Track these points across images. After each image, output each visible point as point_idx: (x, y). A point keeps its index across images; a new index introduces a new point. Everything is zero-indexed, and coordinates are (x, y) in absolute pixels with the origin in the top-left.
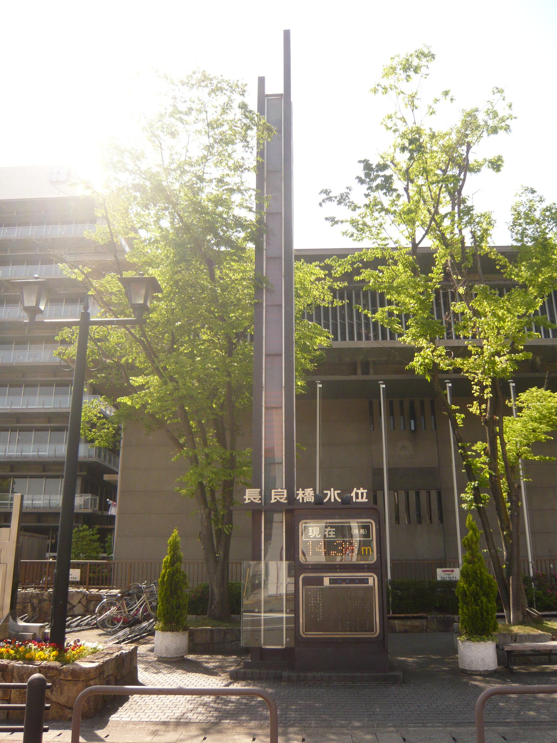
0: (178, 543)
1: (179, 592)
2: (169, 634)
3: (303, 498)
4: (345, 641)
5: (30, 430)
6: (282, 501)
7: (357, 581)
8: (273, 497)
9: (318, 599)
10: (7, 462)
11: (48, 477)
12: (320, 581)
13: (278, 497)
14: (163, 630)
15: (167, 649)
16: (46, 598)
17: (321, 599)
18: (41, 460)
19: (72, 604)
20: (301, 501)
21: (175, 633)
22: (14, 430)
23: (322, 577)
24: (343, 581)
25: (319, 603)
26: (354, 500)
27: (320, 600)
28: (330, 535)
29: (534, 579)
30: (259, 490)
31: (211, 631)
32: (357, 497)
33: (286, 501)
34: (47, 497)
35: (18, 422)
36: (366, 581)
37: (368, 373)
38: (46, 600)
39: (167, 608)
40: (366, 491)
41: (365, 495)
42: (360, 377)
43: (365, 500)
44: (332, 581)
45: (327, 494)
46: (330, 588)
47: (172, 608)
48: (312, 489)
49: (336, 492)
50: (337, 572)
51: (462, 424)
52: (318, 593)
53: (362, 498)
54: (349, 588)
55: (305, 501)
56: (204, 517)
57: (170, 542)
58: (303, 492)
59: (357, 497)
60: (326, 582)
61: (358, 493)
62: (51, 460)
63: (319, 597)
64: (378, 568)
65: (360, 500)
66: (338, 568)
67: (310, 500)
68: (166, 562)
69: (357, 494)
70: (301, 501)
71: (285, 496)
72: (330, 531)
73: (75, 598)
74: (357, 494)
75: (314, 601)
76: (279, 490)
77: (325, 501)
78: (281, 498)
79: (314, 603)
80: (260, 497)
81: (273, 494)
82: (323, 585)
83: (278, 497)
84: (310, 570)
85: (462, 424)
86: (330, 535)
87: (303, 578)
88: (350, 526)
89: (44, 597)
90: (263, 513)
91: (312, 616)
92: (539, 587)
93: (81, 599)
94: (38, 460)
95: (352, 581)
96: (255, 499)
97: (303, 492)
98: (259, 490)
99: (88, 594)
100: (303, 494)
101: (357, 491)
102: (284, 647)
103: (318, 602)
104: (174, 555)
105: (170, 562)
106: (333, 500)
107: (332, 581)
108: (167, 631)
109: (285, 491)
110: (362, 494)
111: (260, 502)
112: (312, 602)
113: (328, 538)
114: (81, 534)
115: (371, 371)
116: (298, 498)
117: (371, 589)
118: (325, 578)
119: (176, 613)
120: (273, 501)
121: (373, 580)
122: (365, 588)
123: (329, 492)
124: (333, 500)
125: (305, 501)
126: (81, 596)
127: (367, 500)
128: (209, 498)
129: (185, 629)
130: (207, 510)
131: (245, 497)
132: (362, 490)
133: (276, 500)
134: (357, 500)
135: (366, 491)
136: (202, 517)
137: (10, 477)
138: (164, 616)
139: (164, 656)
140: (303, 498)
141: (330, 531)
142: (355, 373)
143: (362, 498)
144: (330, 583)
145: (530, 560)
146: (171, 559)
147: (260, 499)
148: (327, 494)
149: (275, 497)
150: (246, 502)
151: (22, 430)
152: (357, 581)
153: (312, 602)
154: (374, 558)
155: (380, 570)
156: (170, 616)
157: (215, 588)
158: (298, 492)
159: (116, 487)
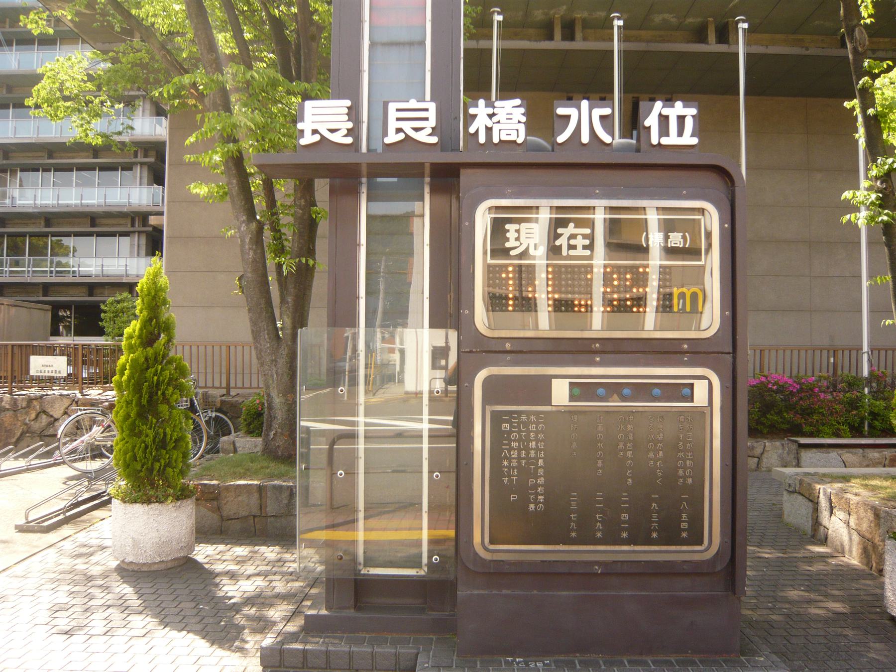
0: (162, 289)
1: (163, 408)
2: (138, 508)
3: (489, 130)
4: (614, 571)
5: (68, 168)
6: (423, 137)
7: (657, 392)
8: (393, 125)
9: (533, 444)
10: (39, 213)
11: (100, 234)
12: (540, 390)
13: (407, 126)
14: (129, 499)
15: (136, 544)
16: (8, 407)
17: (541, 445)
18: (87, 209)
19: (52, 416)
20: (482, 139)
21: (154, 506)
22: (46, 169)
23: (548, 379)
24: (614, 389)
25: (537, 459)
26: (654, 140)
27: (537, 449)
28: (574, 247)
29: (869, 381)
30: (348, 103)
31: (260, 489)
32: (664, 130)
33: (434, 140)
34: (99, 261)
35: (50, 156)
36: (684, 391)
37: (572, 38)
38: (8, 409)
39: (134, 447)
40: (694, 111)
41: (689, 124)
42: (558, 44)
43: (688, 139)
44: (581, 390)
45: (568, 117)
46: (571, 413)
47: (146, 447)
48: (518, 102)
49: (598, 112)
50: (593, 364)
51: (870, 16)
52: (533, 427)
53: (680, 133)
54: (633, 413)
55: (496, 140)
56: (247, 240)
57: (142, 290)
58: (490, 111)
59: (664, 130)
60: (560, 392)
61: (667, 117)
62: (100, 210)
63: (537, 440)
64: (723, 353)
65: (673, 139)
66: (596, 352)
67: (513, 138)
68: (130, 337)
69: (664, 120)
70: (482, 139)
71: (432, 122)
72: (573, 236)
73: (57, 406)
74: (664, 120)
75: (519, 450)
76: (413, 104)
77: (561, 139)
78: (417, 130)
79: (519, 458)
80: (350, 125)
81: (392, 115)
82: (548, 402)
83: (407, 126)
84: (509, 357)
85: (870, 16)
86: (574, 247)
87: (487, 382)
88: (646, 219)
89: (3, 404)
90: (364, 180)
91: (513, 497)
92: (875, 395)
93: (67, 408)
94: (81, 210)
95: (642, 391)
96: (332, 131)
97: (490, 111)
98: (348, 103)
99: (79, 399)
100: (491, 116)
101: (665, 112)
102: (423, 573)
103: (532, 454)
104: (151, 320)
105: (140, 337)
106: (585, 138)
107: (577, 391)
108: (135, 501)
109: (432, 106)
110: (681, 119)
111: (349, 140)
112: (514, 454)
113: (569, 257)
114: (119, 306)
115: (579, 35)
116: (472, 130)
117: (702, 415)
118: (554, 381)
119: (157, 459)
120: (392, 138)
121: (706, 389)
122: (682, 412)
123: (572, 111)
124: (585, 138)
125: (496, 140)
126: (66, 402)
127: (695, 141)
128: (259, 202)
129: (183, 494)
130: (254, 225)
131: (300, 126)
132: (679, 108)
133: (401, 136)
134: (665, 141)
135: (694, 111)
136: (243, 241)
137: (46, 235)
138: (127, 466)
139: (130, 559)
140: (489, 130)
141: (573, 236)
142: (551, 38)
143: (680, 133)
144: (572, 398)
145: (865, 348)
146: (141, 329)
147: (350, 132)
148: (568, 117)
149: (401, 124)
150: (303, 142)
151: (59, 169)
152: (626, 391)
153: (514, 454)
154: (711, 320)
155: (729, 358)
156: (142, 467)
157: (274, 394)
158: (472, 111)
159: (162, 231)
